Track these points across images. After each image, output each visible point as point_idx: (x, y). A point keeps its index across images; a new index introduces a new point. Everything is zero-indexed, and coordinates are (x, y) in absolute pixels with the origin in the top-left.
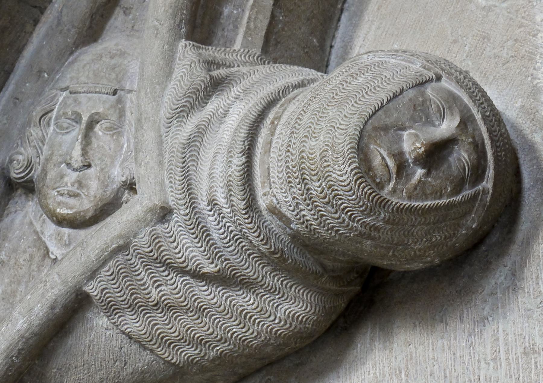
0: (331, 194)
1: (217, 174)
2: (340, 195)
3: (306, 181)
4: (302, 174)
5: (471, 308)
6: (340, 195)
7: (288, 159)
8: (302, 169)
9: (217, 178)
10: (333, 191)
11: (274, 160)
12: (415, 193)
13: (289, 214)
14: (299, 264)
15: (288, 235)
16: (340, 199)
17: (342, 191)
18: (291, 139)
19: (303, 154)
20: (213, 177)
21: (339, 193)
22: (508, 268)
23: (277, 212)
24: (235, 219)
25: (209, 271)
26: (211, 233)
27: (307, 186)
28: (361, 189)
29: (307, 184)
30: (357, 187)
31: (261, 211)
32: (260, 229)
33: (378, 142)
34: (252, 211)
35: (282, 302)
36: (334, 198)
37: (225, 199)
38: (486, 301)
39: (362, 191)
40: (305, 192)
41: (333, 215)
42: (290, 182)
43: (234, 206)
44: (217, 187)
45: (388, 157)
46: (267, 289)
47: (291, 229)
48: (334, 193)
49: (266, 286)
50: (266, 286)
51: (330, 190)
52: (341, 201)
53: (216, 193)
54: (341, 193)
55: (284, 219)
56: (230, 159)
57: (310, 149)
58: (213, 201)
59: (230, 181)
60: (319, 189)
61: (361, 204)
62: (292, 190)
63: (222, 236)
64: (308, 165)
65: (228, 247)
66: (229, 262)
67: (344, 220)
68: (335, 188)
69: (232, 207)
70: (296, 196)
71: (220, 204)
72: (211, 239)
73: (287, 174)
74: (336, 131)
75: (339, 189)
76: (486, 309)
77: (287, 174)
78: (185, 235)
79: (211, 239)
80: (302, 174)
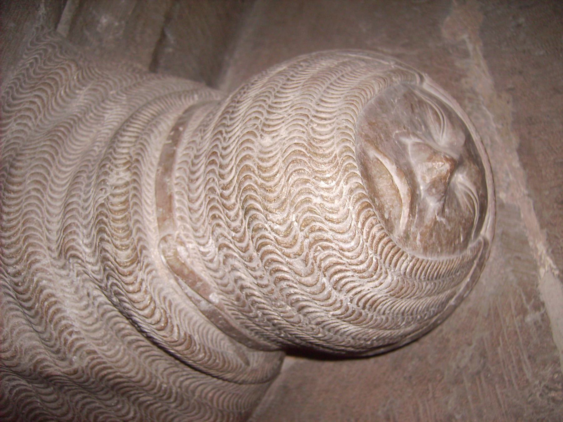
0: (306, 237)
1: (79, 205)
2: (327, 240)
3: (252, 212)
4: (245, 201)
5: (428, 401)
6: (327, 240)
7: (211, 175)
8: (245, 190)
9: (78, 212)
10: (312, 231)
11: (183, 182)
12: (431, 242)
13: (205, 276)
14: (215, 360)
15: (203, 312)
16: (324, 248)
17: (331, 233)
18: (217, 143)
19: (249, 163)
20: (73, 210)
21: (326, 236)
22: (473, 346)
23: (186, 272)
24: (110, 283)
25: (59, 373)
26: (64, 308)
27: (255, 223)
28: (366, 229)
29: (254, 218)
30: (360, 226)
31: (156, 270)
32: (155, 302)
33: (380, 148)
34: (141, 270)
35: (180, 413)
36: (310, 246)
37: (91, 247)
38: (449, 392)
39: (368, 233)
40: (249, 234)
41: (304, 280)
42: (214, 217)
43: (108, 260)
44: (77, 226)
45: (398, 175)
46: (158, 395)
47: (209, 302)
48: (313, 235)
49: (155, 391)
50: (155, 391)
51: (307, 229)
52: (327, 252)
53: (75, 237)
54: (329, 235)
55: (199, 284)
56: (103, 178)
57: (261, 152)
58: (68, 250)
59: (101, 214)
60: (283, 228)
61: (361, 258)
62: (218, 231)
63: (84, 313)
64: (260, 181)
65: (95, 331)
66: (95, 356)
67: (323, 288)
68: (318, 224)
69: (102, 262)
70: (227, 242)
71: (81, 256)
72: (64, 318)
73: (209, 203)
74: (311, 121)
75: (326, 228)
76: (450, 402)
77: (209, 203)
78: (18, 310)
79: (64, 318)
80: (245, 201)
